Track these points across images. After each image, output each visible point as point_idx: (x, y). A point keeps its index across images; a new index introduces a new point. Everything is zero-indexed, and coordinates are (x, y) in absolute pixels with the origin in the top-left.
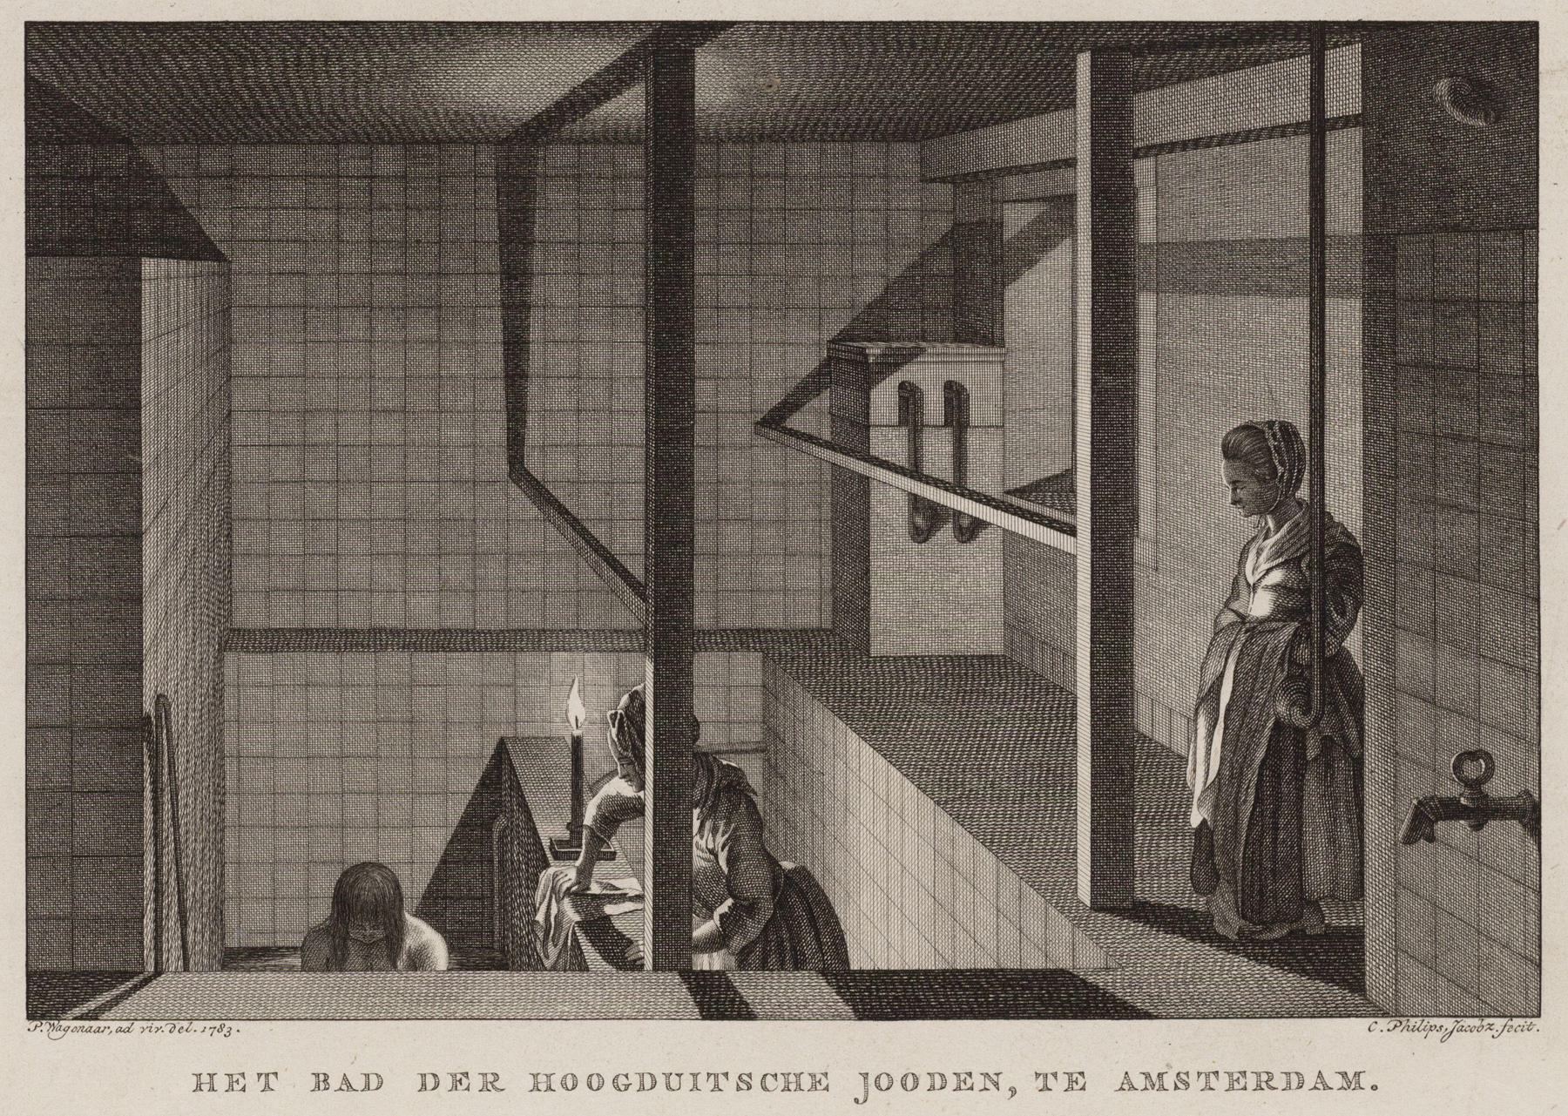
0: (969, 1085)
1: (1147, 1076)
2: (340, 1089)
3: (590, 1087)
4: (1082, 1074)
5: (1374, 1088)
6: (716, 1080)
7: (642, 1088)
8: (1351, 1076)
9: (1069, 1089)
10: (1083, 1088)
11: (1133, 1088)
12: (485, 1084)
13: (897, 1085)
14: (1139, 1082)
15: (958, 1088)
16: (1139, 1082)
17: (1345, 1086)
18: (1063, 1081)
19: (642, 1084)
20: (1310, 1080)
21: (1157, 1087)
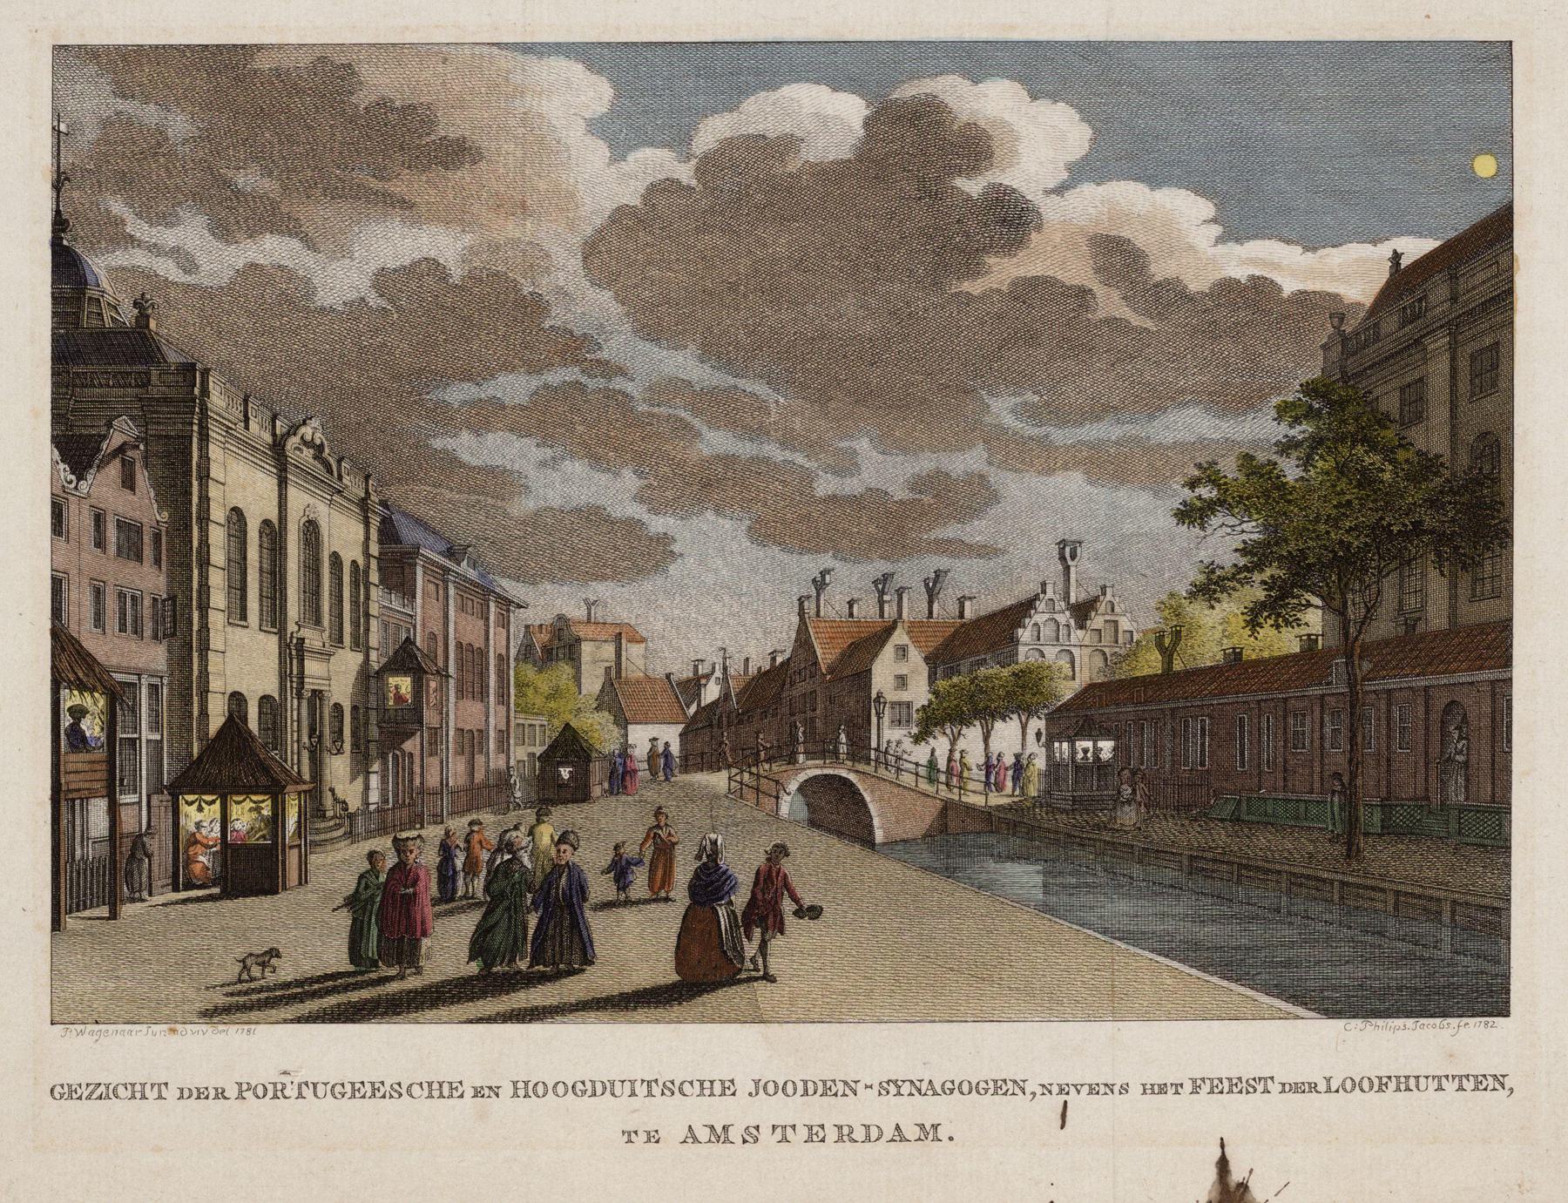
0: (833, 1092)
1: (922, 1126)
2: (685, 1142)
3: (258, 1097)
4: (657, 1131)
5: (951, 1139)
6: (629, 1135)
7: (806, 1093)
8: (928, 1128)
10: (734, 1094)
11: (904, 1139)
12: (217, 1095)
13: (550, 1087)
14: (703, 1134)
15: (199, 1098)
16: (703, 1134)
17: (923, 1137)
18: (803, 1133)
19: (806, 1090)
20: (889, 1132)
21: (722, 1139)
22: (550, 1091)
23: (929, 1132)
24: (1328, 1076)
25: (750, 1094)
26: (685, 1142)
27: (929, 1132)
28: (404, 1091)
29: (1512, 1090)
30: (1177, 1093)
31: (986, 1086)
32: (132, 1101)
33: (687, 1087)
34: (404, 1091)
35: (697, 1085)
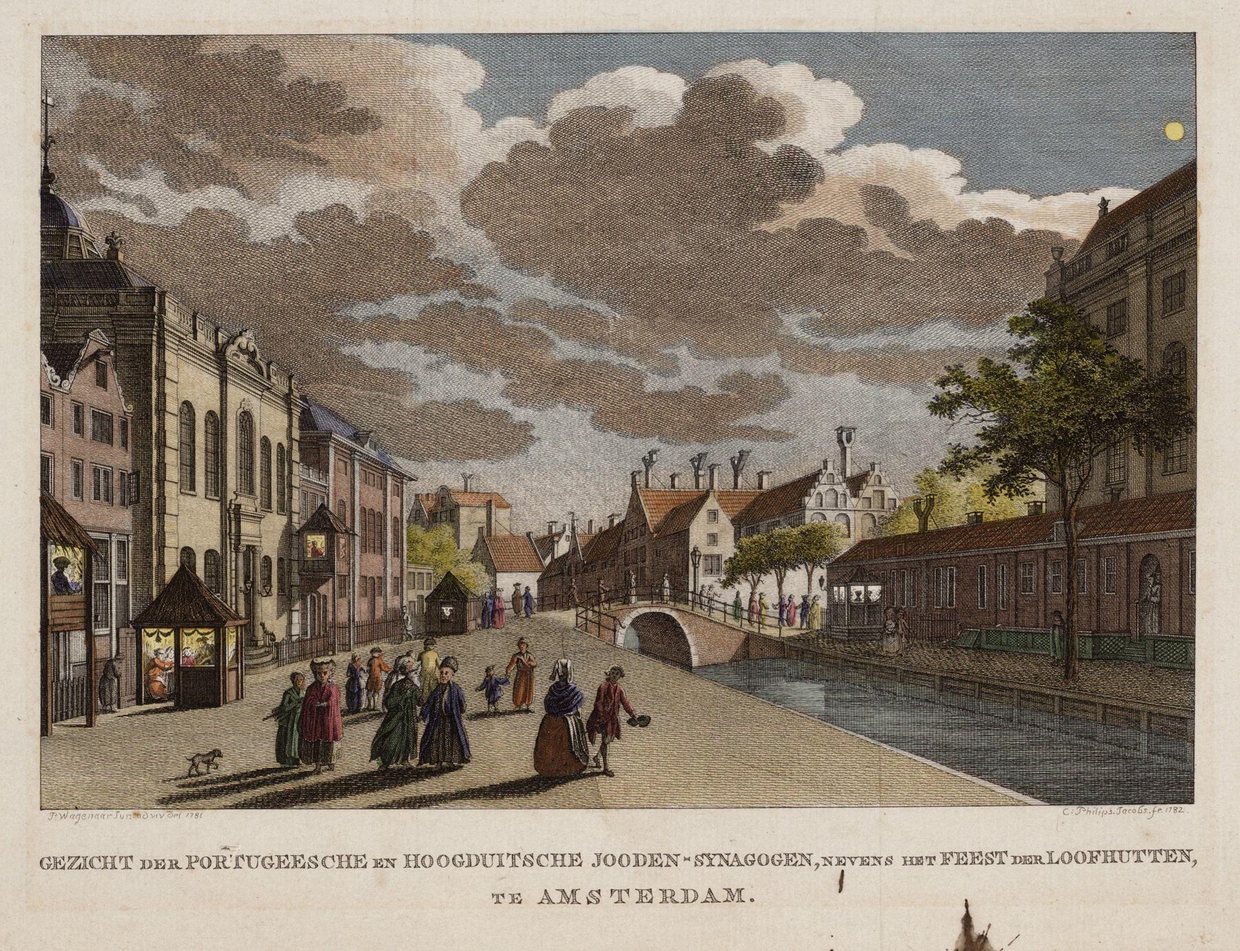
0: (659, 863)
1: (729, 890)
2: (541, 902)
3: (204, 867)
4: (519, 894)
5: (752, 900)
6: (498, 897)
7: (637, 864)
8: (734, 891)
9: (640, 901)
10: (580, 865)
11: (715, 901)
13: (435, 859)
14: (556, 896)
15: (157, 868)
16: (556, 896)
17: (730, 899)
18: (635, 896)
19: (637, 862)
20: (703, 895)
21: (571, 901)
22: (435, 862)
23: (734, 895)
24: (1050, 850)
25: (593, 865)
26: (541, 902)
27: (734, 895)
28: (319, 863)
29: (1195, 862)
30: (931, 864)
31: (779, 859)
32: (105, 870)
33: (543, 859)
34: (319, 863)
35: (551, 857)
